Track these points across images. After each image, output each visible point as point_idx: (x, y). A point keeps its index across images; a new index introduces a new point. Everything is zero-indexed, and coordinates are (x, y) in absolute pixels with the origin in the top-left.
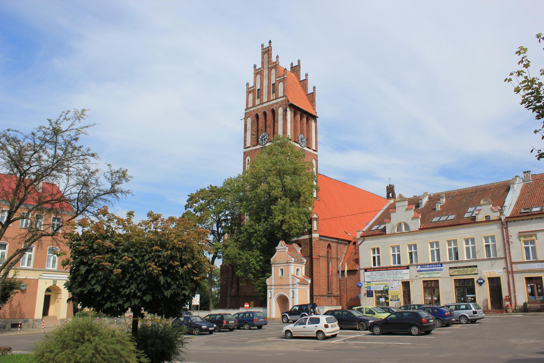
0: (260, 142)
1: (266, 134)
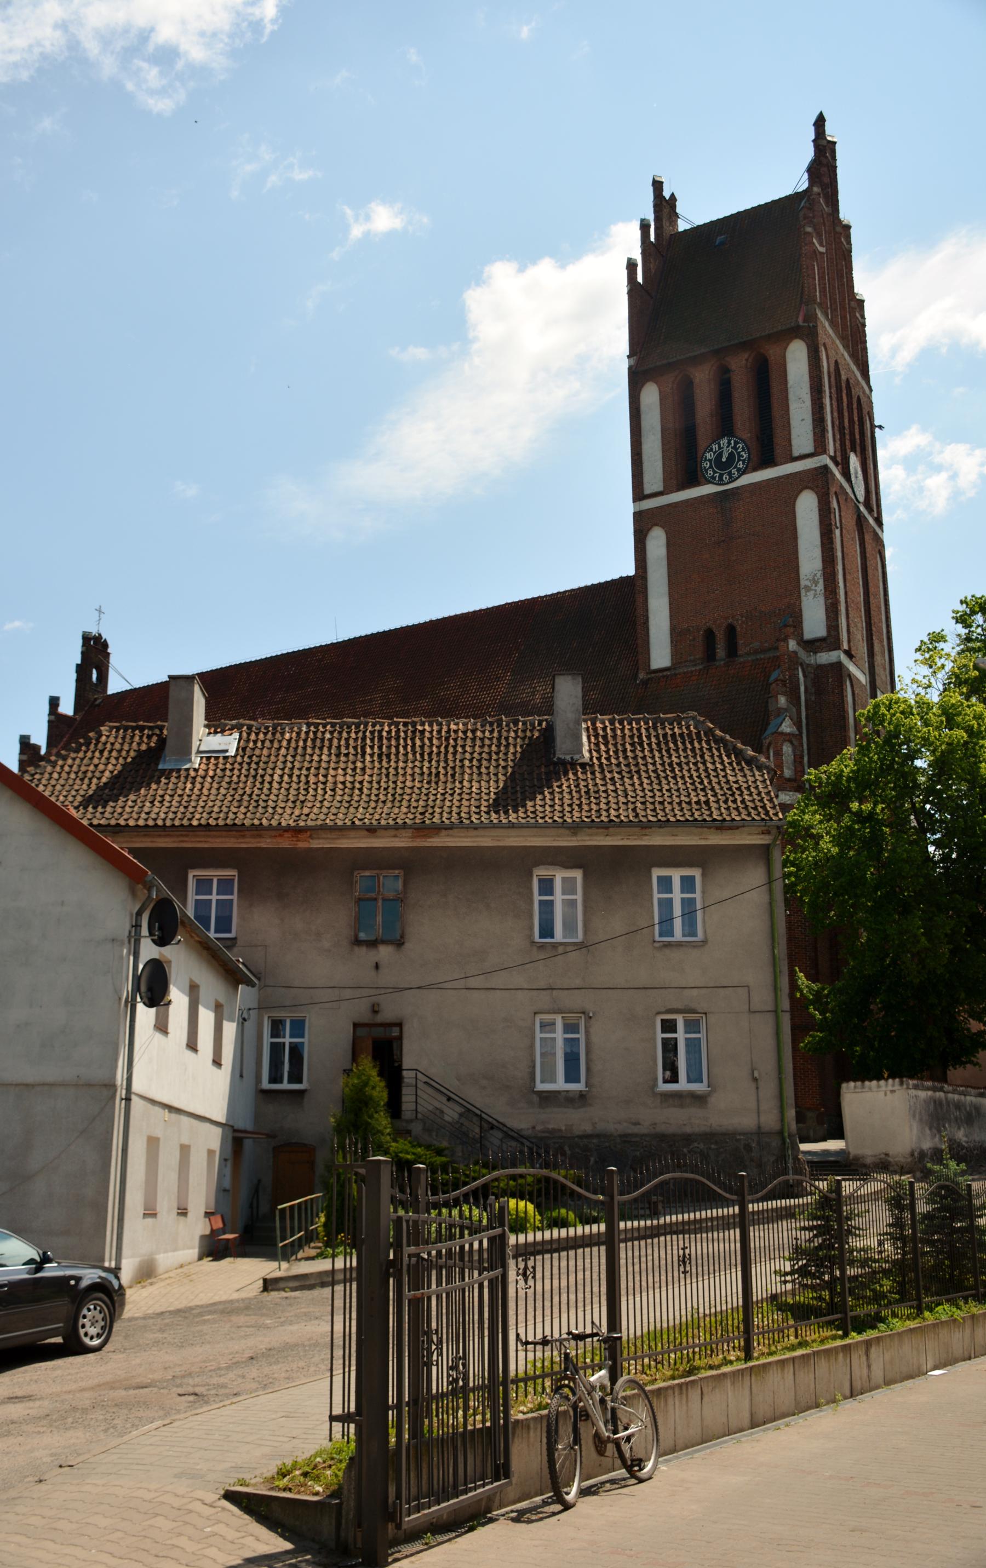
0: (710, 472)
1: (736, 443)
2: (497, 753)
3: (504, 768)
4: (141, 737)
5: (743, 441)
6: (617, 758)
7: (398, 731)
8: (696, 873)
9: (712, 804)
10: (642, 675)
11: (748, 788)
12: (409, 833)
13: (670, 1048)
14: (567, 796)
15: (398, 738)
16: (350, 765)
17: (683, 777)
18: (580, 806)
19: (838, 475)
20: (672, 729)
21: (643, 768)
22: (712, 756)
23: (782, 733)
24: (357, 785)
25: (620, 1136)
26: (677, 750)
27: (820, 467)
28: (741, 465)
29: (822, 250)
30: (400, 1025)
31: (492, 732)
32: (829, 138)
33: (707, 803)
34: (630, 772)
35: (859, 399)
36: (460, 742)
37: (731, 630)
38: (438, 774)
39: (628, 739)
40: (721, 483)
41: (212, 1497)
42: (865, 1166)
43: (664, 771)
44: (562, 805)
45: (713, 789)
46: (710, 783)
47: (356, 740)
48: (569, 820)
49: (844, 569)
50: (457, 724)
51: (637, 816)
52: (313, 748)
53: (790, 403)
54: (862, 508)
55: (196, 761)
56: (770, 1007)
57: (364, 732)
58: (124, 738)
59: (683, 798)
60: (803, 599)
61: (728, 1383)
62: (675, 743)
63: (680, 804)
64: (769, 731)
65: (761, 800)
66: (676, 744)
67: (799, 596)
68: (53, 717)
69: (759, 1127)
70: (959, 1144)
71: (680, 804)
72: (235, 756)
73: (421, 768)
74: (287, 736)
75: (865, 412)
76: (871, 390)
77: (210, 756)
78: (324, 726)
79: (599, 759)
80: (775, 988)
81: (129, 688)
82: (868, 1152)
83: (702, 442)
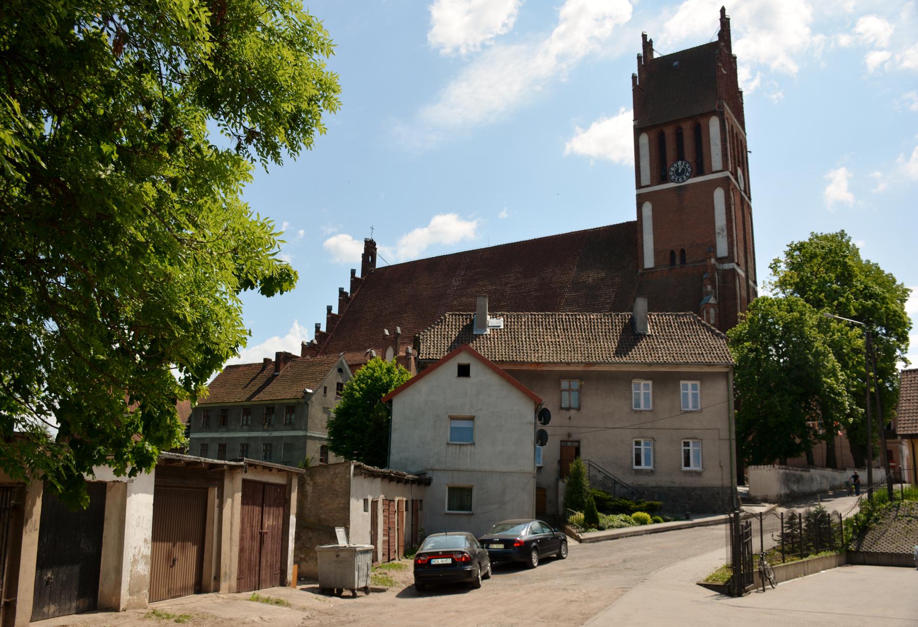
0: (673, 177)
1: (685, 164)
2: (612, 329)
3: (616, 336)
4: (463, 319)
5: (689, 163)
6: (662, 332)
7: (569, 319)
8: (698, 383)
9: (705, 355)
10: (640, 271)
11: (718, 347)
12: (583, 365)
13: (687, 453)
14: (644, 350)
15: (570, 322)
16: (553, 334)
17: (690, 342)
18: (651, 354)
19: (733, 180)
20: (683, 319)
21: (673, 337)
22: (701, 332)
23: (710, 304)
24: (558, 343)
25: (668, 488)
26: (686, 329)
28: (688, 174)
29: (725, 72)
30: (579, 442)
31: (608, 319)
32: (727, 17)
33: (702, 354)
34: (668, 339)
35: (741, 141)
36: (596, 324)
37: (683, 251)
38: (589, 338)
39: (665, 324)
40: (678, 182)
41: (695, 584)
42: (757, 500)
43: (682, 339)
44: (643, 354)
45: (704, 348)
46: (702, 344)
47: (552, 322)
48: (648, 361)
49: (736, 224)
50: (593, 315)
51: (675, 360)
52: (535, 325)
54: (743, 193)
55: (488, 331)
56: (728, 438)
57: (555, 319)
58: (456, 319)
59: (692, 352)
60: (717, 238)
61: (790, 567)
62: (685, 326)
63: (691, 354)
64: (703, 303)
65: (724, 353)
66: (686, 327)
67: (715, 237)
68: (353, 279)
69: (722, 485)
70: (794, 492)
71: (691, 354)
72: (504, 329)
73: (582, 335)
74: (523, 320)
75: (744, 146)
76: (746, 135)
77: (495, 329)
78: (538, 316)
79: (655, 333)
80: (730, 430)
81: (387, 265)
82: (759, 494)
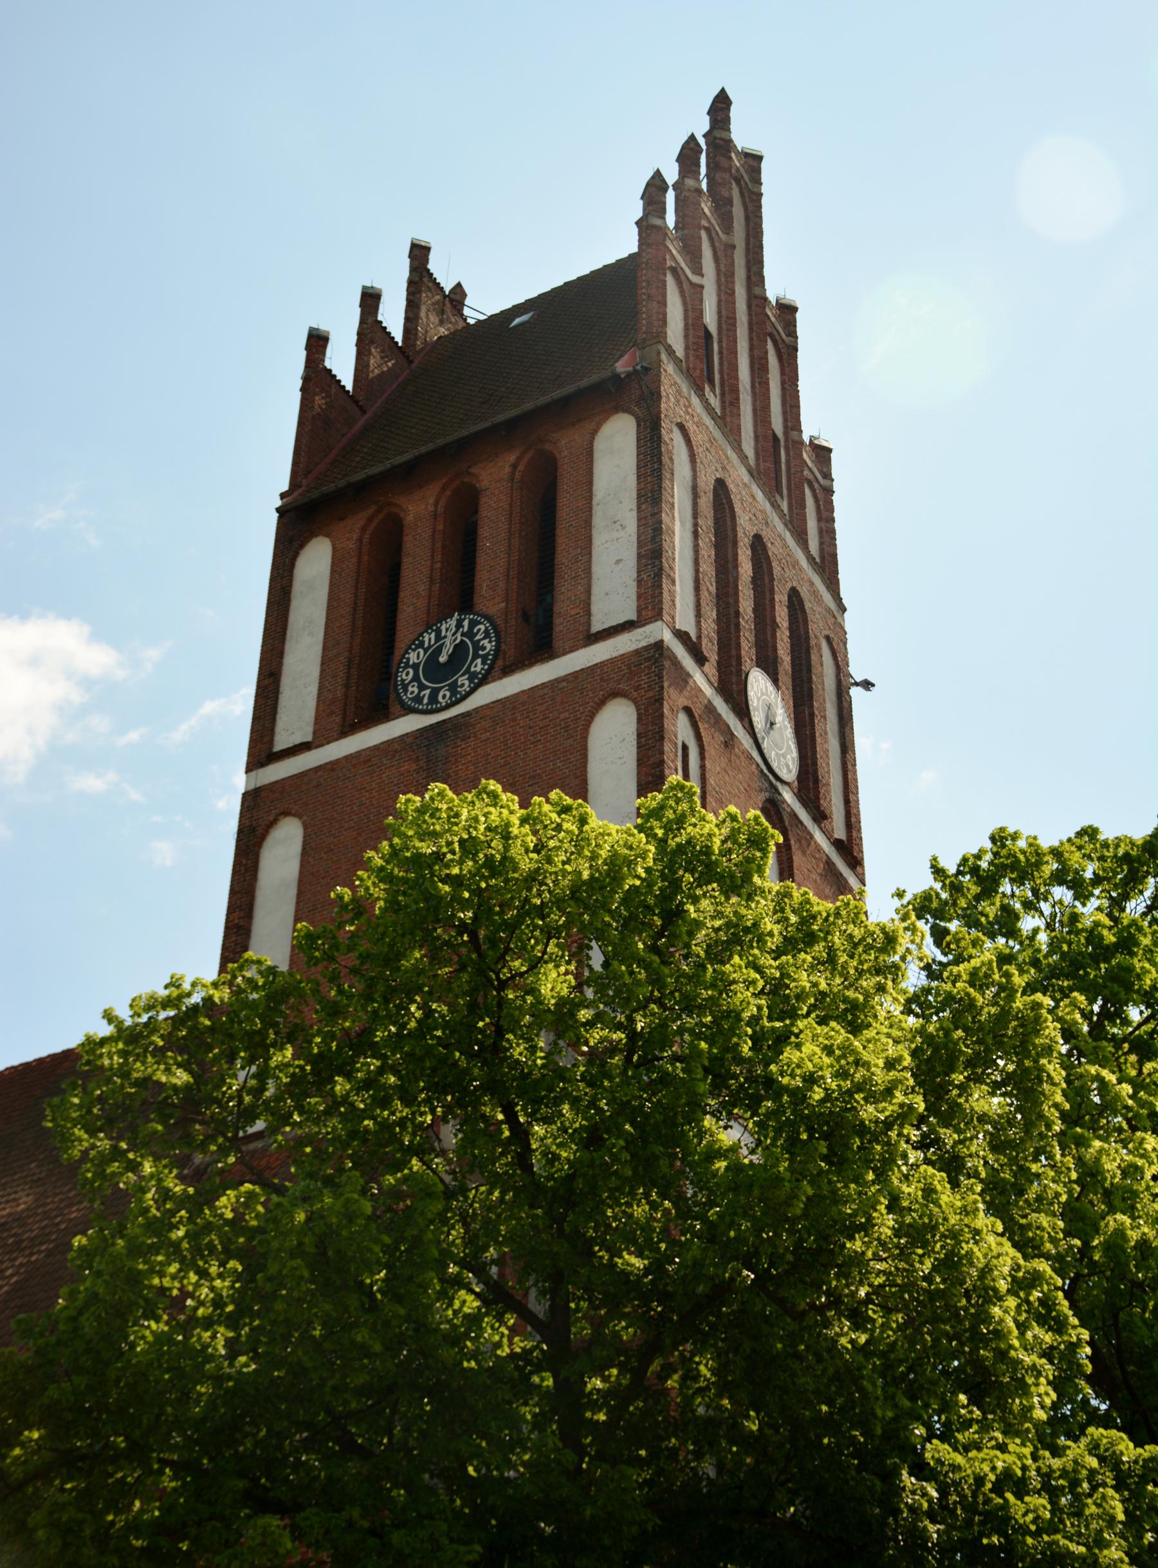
0: (413, 689)
1: (473, 623)
5: (488, 618)
27: (646, 648)
35: (795, 600)
53: (595, 533)
83: (404, 635)
